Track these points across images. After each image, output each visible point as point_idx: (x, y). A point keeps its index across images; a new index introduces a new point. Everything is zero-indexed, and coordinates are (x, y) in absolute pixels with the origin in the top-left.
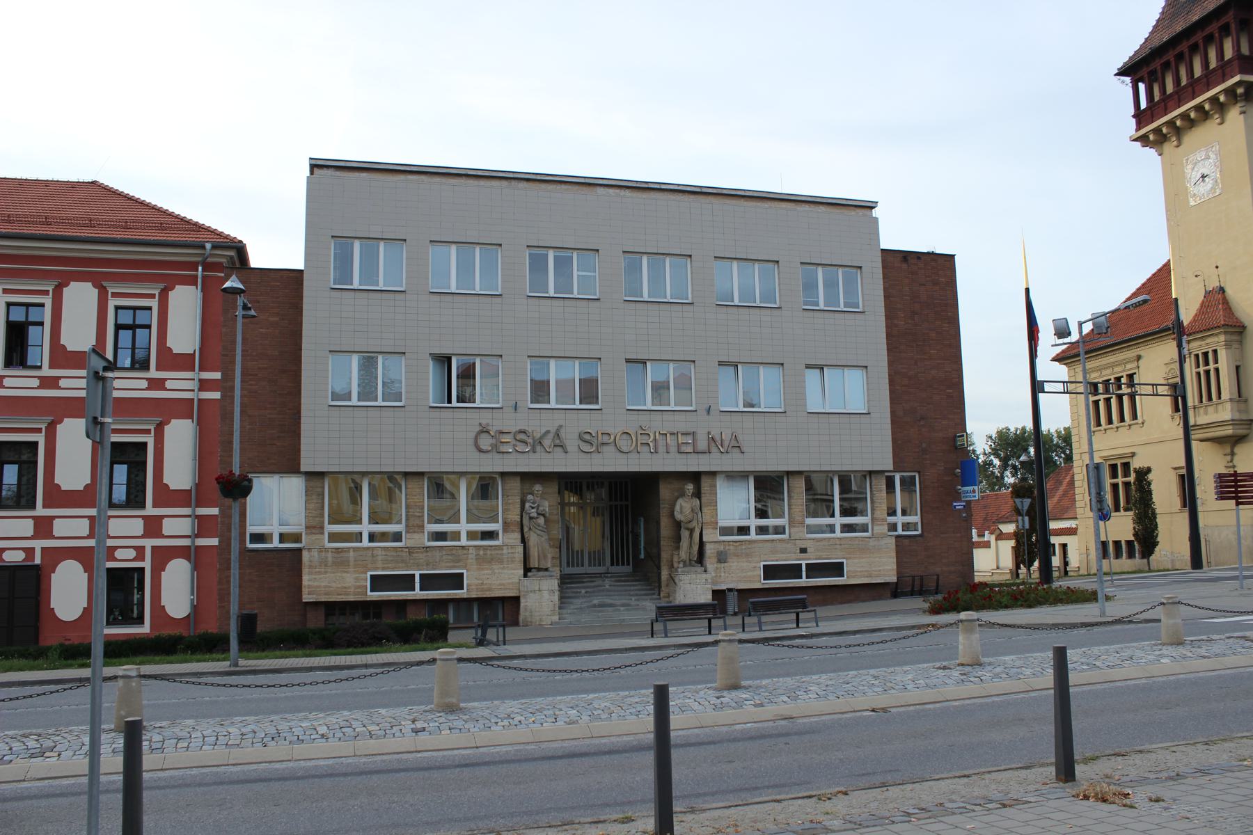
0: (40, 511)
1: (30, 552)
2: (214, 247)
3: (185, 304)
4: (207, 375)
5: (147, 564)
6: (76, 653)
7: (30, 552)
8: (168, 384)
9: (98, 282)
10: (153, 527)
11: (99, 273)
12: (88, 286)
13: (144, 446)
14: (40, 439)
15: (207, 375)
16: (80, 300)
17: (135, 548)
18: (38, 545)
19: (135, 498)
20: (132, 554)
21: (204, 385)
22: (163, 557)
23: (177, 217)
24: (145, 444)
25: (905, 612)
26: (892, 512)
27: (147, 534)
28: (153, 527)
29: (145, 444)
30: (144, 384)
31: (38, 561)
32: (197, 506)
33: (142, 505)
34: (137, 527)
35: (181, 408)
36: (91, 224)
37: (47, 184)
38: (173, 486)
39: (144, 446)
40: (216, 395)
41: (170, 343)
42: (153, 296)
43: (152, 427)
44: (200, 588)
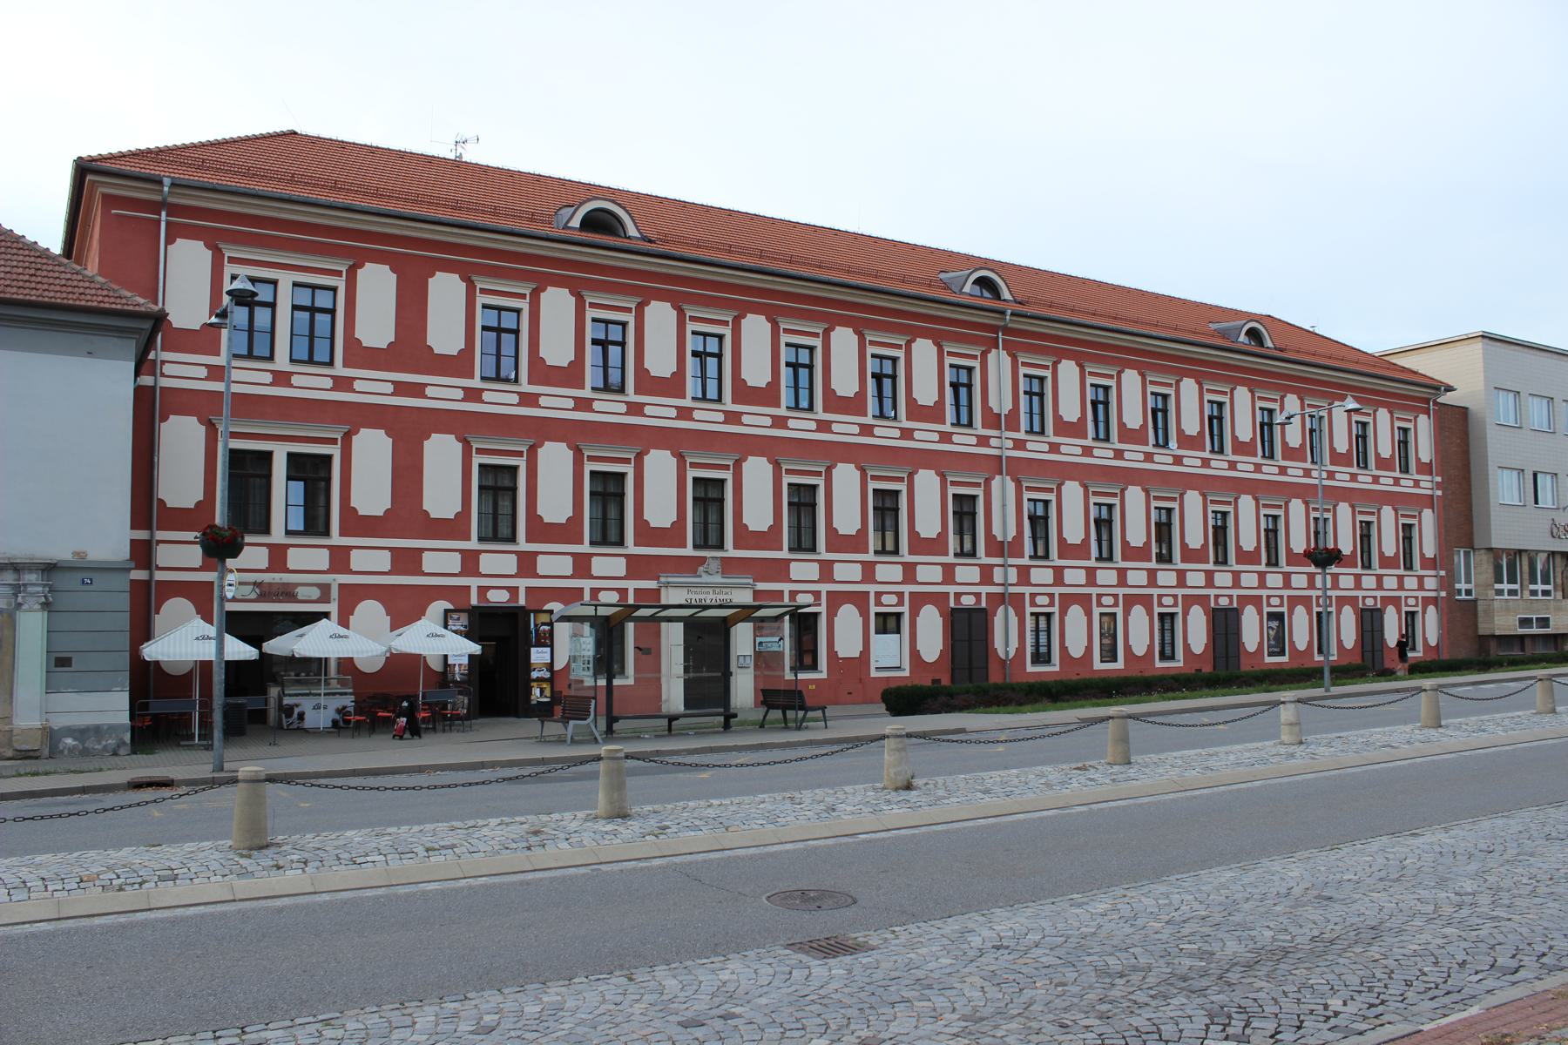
1: (514, 591)
2: (173, 185)
8: (357, 385)
9: (938, 339)
13: (328, 459)
14: (335, 451)
17: (318, 585)
18: (523, 583)
19: (316, 524)
20: (315, 593)
23: (202, 145)
26: (1533, 581)
27: (333, 569)
28: (340, 561)
29: (329, 458)
32: (1010, 556)
33: (326, 533)
34: (321, 559)
35: (1429, 501)
36: (335, 187)
37: (708, 209)
38: (363, 511)
39: (328, 459)
41: (359, 333)
42: (523, 296)
43: (632, 457)
44: (1446, 626)
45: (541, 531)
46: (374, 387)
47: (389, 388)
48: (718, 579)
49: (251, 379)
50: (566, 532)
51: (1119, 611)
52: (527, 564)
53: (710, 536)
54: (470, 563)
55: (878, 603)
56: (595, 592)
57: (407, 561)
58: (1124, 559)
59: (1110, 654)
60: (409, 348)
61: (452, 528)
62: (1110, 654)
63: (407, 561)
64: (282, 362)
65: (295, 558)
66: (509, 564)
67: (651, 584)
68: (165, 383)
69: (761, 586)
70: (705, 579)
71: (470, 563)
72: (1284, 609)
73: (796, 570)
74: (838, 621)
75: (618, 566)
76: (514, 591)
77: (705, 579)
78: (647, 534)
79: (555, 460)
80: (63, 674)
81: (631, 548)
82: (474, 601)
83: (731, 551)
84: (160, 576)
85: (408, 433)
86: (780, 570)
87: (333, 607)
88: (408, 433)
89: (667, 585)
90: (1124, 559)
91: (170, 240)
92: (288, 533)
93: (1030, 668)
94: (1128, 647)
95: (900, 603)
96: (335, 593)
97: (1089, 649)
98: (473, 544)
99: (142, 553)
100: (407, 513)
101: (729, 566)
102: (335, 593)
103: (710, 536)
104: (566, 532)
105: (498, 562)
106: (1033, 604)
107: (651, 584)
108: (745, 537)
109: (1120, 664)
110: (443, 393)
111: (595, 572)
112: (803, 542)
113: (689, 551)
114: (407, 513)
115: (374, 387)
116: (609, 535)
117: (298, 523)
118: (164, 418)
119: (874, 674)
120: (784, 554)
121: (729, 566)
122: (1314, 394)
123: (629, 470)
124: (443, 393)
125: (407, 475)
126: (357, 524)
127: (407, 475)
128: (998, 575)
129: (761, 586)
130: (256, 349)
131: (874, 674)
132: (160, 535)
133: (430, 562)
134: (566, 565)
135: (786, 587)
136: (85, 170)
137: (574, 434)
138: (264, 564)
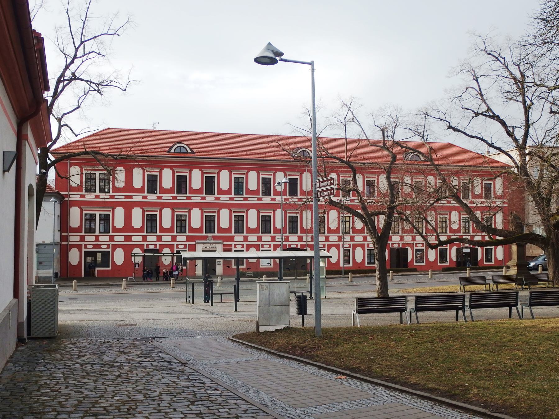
0: (158, 234)
3: (499, 182)
4: (505, 200)
5: (110, 250)
6: (415, 270)
7: (156, 245)
10: (112, 238)
11: (172, 165)
12: (254, 172)
14: (272, 215)
15: (505, 200)
16: (253, 175)
18: (158, 243)
19: (106, 231)
20: (106, 246)
21: (504, 203)
22: (115, 247)
24: (156, 215)
25: (447, 282)
27: (110, 241)
28: (112, 238)
29: (156, 215)
30: (185, 198)
31: (158, 248)
34: (107, 238)
40: (507, 205)
45: (249, 231)
46: (120, 197)
47: (124, 197)
48: (212, 241)
49: (90, 197)
50: (256, 231)
51: (351, 249)
52: (159, 239)
53: (210, 229)
54: (144, 239)
55: (368, 246)
56: (177, 245)
57: (128, 238)
58: (353, 233)
59: (347, 261)
60: (129, 187)
61: (140, 230)
62: (347, 261)
63: (128, 238)
64: (97, 192)
65: (101, 238)
66: (296, 239)
67: (193, 243)
68: (70, 199)
69: (225, 243)
70: (208, 241)
71: (144, 239)
72: (424, 248)
73: (236, 239)
74: (116, 253)
75: (184, 239)
76: (399, 244)
77: (208, 241)
78: (192, 230)
79: (253, 213)
80: (41, 266)
81: (188, 234)
82: (145, 248)
83: (216, 234)
84: (70, 243)
85: (128, 207)
86: (232, 239)
87: (326, 248)
88: (128, 207)
89: (197, 243)
90: (353, 233)
91: (71, 166)
92: (100, 232)
93: (366, 265)
94: (354, 260)
95: (350, 247)
96: (111, 246)
97: (339, 260)
98: (145, 234)
99: (64, 238)
100: (128, 227)
101: (215, 238)
102: (111, 246)
103: (210, 229)
104: (256, 231)
105: (152, 238)
106: (416, 246)
107: (193, 243)
108: (221, 230)
109: (351, 265)
110: (137, 197)
111: (86, 240)
112: (239, 230)
113: (204, 234)
114: (128, 227)
115: (120, 197)
116: (182, 231)
117: (102, 230)
118: (71, 207)
119: (261, 267)
120: (233, 234)
121: (215, 238)
122: (85, 164)
123: (244, 214)
124: (137, 197)
125: (128, 218)
126: (116, 230)
127: (128, 218)
128: (304, 239)
129: (225, 243)
130: (91, 190)
131: (261, 267)
132: (70, 234)
133: (134, 239)
134: (255, 239)
135: (233, 243)
136: (4, 152)
137: (285, 207)
138: (94, 240)
